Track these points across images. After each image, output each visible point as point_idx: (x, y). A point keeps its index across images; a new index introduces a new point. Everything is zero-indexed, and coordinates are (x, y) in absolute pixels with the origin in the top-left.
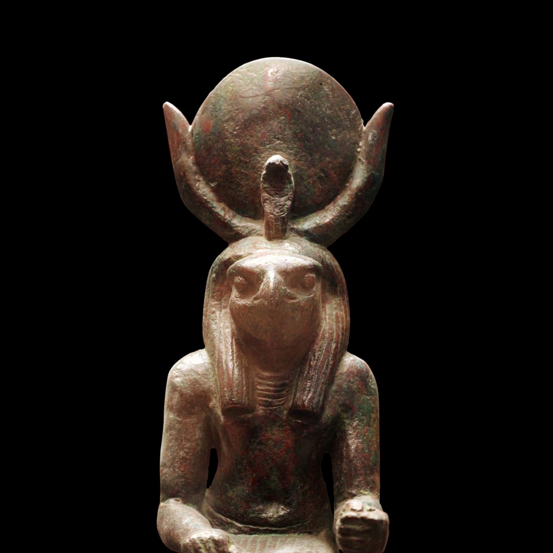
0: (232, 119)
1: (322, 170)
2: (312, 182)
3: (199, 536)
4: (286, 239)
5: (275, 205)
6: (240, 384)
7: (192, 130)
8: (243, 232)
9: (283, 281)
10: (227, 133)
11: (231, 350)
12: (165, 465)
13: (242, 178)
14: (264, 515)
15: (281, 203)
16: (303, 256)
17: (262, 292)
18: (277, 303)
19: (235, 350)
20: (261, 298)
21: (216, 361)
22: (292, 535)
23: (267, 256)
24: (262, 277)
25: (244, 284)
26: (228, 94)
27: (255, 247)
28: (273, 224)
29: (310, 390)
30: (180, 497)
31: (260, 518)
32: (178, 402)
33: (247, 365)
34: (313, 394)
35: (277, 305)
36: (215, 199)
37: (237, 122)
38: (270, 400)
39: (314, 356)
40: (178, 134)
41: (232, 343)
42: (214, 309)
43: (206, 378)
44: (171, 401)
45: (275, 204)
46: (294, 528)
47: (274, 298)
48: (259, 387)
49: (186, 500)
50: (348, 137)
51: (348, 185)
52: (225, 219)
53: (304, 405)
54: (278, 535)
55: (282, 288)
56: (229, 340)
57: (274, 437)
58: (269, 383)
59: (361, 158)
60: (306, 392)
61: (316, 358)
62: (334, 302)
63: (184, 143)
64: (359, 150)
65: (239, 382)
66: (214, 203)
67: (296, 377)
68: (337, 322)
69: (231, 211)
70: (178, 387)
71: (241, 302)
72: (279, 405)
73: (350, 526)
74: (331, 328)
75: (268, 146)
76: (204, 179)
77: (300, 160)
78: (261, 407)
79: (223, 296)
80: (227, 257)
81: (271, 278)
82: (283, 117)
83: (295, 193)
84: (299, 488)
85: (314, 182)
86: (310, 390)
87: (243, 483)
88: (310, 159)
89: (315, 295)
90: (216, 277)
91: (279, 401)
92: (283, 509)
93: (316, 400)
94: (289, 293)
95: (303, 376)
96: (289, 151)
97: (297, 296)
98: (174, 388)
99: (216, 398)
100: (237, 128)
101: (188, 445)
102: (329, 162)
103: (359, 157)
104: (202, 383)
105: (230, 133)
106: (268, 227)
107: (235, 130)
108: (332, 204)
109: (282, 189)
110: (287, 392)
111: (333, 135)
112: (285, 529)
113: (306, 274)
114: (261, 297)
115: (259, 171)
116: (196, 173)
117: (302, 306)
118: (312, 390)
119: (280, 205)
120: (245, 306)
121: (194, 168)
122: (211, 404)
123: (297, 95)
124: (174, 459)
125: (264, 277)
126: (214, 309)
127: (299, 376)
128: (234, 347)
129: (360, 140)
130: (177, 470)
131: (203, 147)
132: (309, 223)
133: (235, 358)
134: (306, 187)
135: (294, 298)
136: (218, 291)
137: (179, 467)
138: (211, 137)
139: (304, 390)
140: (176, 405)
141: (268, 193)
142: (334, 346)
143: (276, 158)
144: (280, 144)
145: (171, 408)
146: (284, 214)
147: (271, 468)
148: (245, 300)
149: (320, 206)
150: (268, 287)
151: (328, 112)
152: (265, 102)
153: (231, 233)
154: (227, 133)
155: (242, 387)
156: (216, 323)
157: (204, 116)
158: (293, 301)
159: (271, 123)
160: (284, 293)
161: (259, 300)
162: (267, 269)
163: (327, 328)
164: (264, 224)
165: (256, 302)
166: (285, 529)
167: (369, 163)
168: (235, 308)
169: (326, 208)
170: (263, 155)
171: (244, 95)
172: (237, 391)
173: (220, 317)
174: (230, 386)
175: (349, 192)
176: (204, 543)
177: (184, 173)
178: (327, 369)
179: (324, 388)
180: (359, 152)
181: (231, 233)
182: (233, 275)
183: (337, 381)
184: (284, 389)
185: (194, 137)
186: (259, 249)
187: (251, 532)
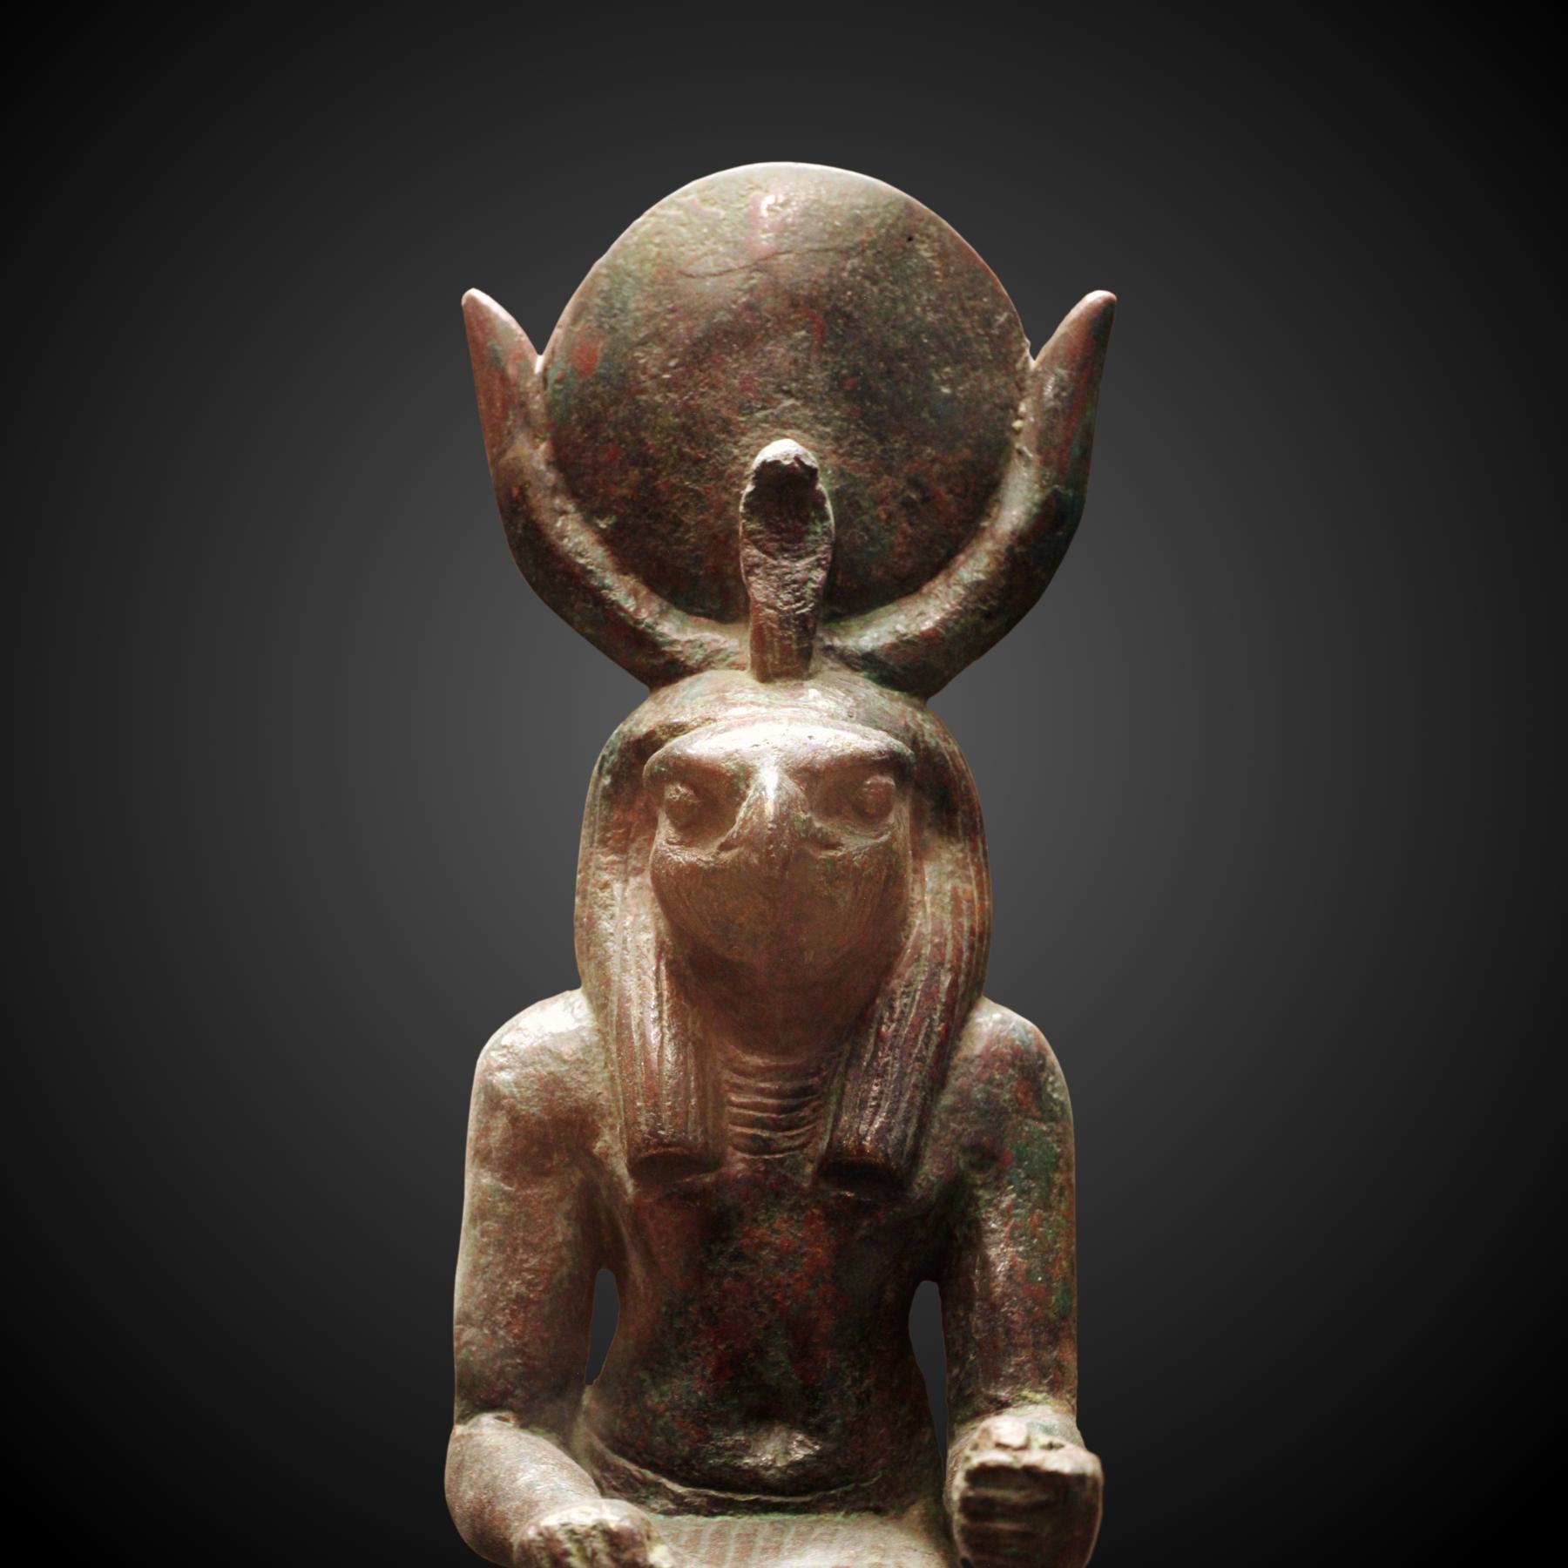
0: (658, 336)
1: (914, 483)
2: (884, 516)
3: (565, 1520)
4: (810, 677)
5: (779, 581)
6: (680, 1090)
7: (545, 369)
8: (688, 658)
9: (802, 796)
10: (643, 378)
11: (654, 993)
12: (467, 1319)
13: (685, 505)
14: (747, 1460)
15: (798, 576)
16: (859, 727)
17: (742, 827)
18: (785, 859)
19: (666, 993)
20: (741, 844)
21: (612, 1022)
22: (828, 1517)
23: (757, 725)
24: (743, 787)
25: (693, 806)
26: (648, 266)
27: (722, 700)
28: (773, 636)
29: (878, 1106)
30: (511, 1408)
31: (738, 1469)
32: (505, 1141)
33: (700, 1035)
34: (887, 1117)
35: (786, 864)
36: (608, 563)
37: (672, 346)
38: (766, 1134)
39: (892, 1009)
40: (504, 379)
41: (657, 972)
42: (606, 877)
43: (585, 1072)
44: (486, 1137)
45: (780, 577)
46: (833, 1498)
47: (778, 844)
48: (733, 1098)
49: (528, 1419)
50: (987, 387)
51: (985, 524)
52: (638, 622)
53: (861, 1149)
54: (788, 1517)
55: (798, 818)
56: (650, 963)
57: (776, 1240)
58: (762, 1085)
59: (1025, 449)
60: (868, 1113)
61: (896, 1016)
62: (946, 856)
63: (523, 405)
64: (1018, 424)
65: (678, 1084)
66: (608, 574)
67: (841, 1069)
68: (957, 912)
69: (654, 597)
70: (505, 1097)
71: (685, 856)
72: (790, 1149)
73: (992, 1493)
74: (938, 931)
75: (760, 415)
76: (579, 509)
77: (850, 454)
78: (739, 1155)
79: (633, 841)
80: (643, 729)
81: (770, 789)
82: (803, 333)
83: (836, 546)
84: (849, 1383)
85: (890, 516)
86: (878, 1106)
87: (689, 1371)
88: (878, 450)
89: (894, 838)
90: (613, 784)
91: (792, 1138)
92: (802, 1444)
93: (895, 1135)
94: (820, 829)
95: (860, 1065)
96: (821, 428)
97: (843, 840)
98: (494, 1101)
99: (612, 1127)
100: (672, 363)
101: (533, 1262)
102: (934, 460)
103: (1017, 445)
104: (573, 1085)
105: (653, 377)
106: (760, 643)
107: (665, 369)
108: (941, 577)
109: (798, 537)
110: (814, 1110)
111: (944, 383)
112: (807, 1499)
113: (866, 778)
114: (741, 841)
115: (733, 484)
116: (555, 491)
117: (855, 869)
118: (886, 1105)
119: (795, 582)
120: (694, 869)
121: (551, 477)
122: (599, 1146)
123: (843, 269)
124: (493, 1301)
125: (748, 787)
126: (606, 877)
127: (848, 1065)
128: (665, 984)
129: (1022, 398)
130: (502, 1333)
131: (575, 417)
132: (875, 634)
133: (665, 1016)
134: (867, 530)
135: (834, 846)
136: (619, 826)
137: (509, 1324)
138: (600, 389)
139: (863, 1105)
140: (499, 1150)
141: (760, 548)
142: (946, 980)
143: (782, 449)
144: (794, 407)
145: (484, 1158)
146: (804, 606)
147: (767, 1327)
148: (694, 851)
149: (906, 585)
150: (761, 814)
151: (931, 317)
152: (751, 290)
153: (654, 662)
154: (643, 378)
155: (687, 1098)
156: (612, 917)
157: (577, 329)
158: (832, 853)
159: (768, 348)
160: (806, 831)
161: (736, 851)
162: (757, 763)
163: (927, 929)
164: (748, 636)
165: (726, 856)
166: (807, 1499)
167: (1046, 462)
168: (668, 874)
169: (925, 590)
170: (745, 440)
171: (691, 269)
172: (671, 1108)
173: (624, 899)
174: (653, 1095)
176: (577, 1541)
177: (522, 490)
178: (927, 1045)
179: (918, 1101)
180: (1017, 432)
181: (654, 662)
182: (660, 780)
183: (956, 1082)
184: (806, 1104)
185: (549, 390)
186: (734, 705)
187: (712, 1508)
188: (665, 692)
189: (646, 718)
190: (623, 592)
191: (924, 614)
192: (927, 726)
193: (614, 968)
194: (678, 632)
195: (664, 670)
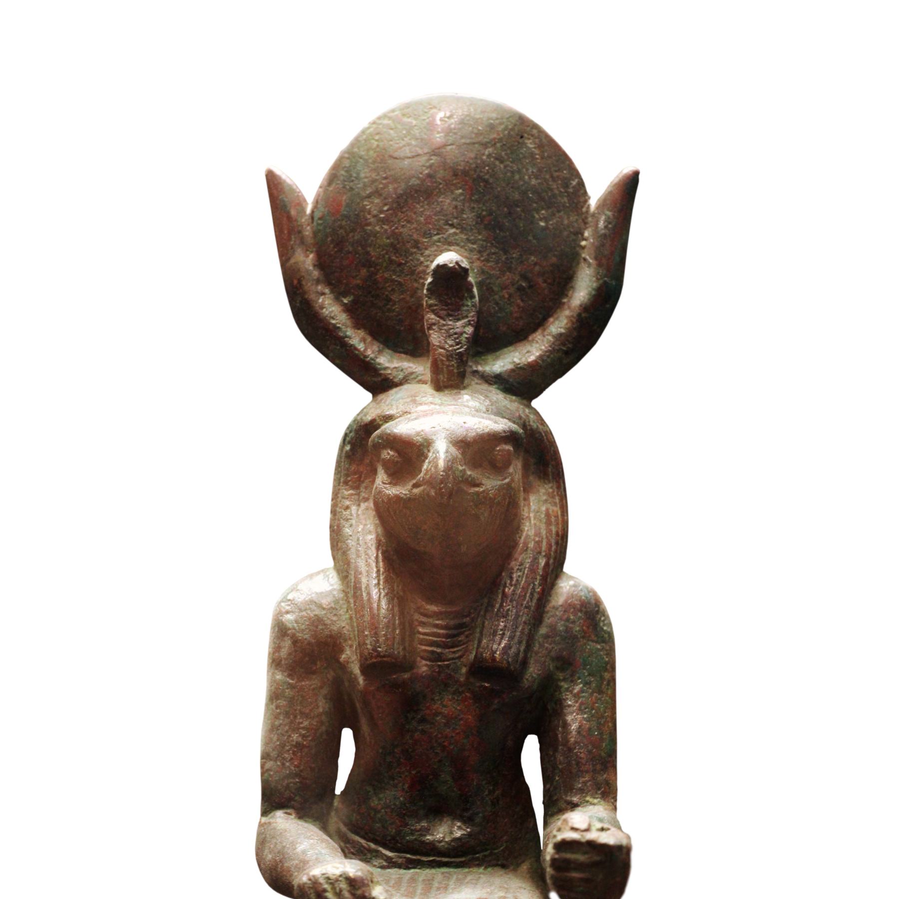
0: (377, 193)
1: (524, 277)
2: (507, 296)
3: (324, 872)
4: (465, 388)
5: (446, 333)
6: (390, 625)
8: (394, 377)
9: (460, 456)
10: (369, 217)
11: (375, 570)
13: (393, 290)
14: (428, 837)
15: (458, 330)
16: (492, 417)
17: (425, 474)
18: (450, 493)
19: (382, 570)
20: (425, 484)
22: (475, 870)
23: (434, 416)
24: (426, 451)
25: (397, 462)
26: (371, 153)
27: (414, 401)
28: (443, 364)
29: (504, 634)
30: (293, 807)
31: (423, 842)
32: (290, 654)
33: (401, 593)
34: (508, 641)
35: (450, 495)
36: (349, 323)
37: (385, 198)
38: (439, 650)
39: (511, 578)
41: (377, 557)
42: (347, 503)
43: (335, 615)
44: (279, 652)
45: (447, 331)
46: (478, 859)
47: (446, 484)
48: (421, 630)
50: (566, 222)
51: (565, 300)
52: (366, 357)
53: (494, 659)
54: (452, 870)
55: (458, 469)
56: (373, 552)
57: (445, 711)
58: (437, 622)
59: (588, 257)
60: (498, 638)
61: (514, 583)
62: (543, 491)
63: (300, 232)
64: (583, 243)
65: (389, 622)
66: (349, 329)
67: (482, 613)
68: (548, 523)
69: (375, 342)
70: (289, 629)
71: (393, 491)
72: (453, 659)
73: (569, 856)
74: (538, 534)
75: (436, 238)
76: (332, 292)
77: (487, 260)
78: (424, 662)
79: (363, 482)
81: (441, 452)
82: (460, 191)
83: (479, 313)
84: (487, 793)
85: (510, 296)
86: (504, 634)
87: (395, 786)
88: (504, 258)
89: (512, 480)
90: (351, 450)
91: (454, 652)
92: (460, 828)
93: (513, 650)
94: (470, 476)
95: (493, 611)
96: (471, 246)
97: (484, 482)
99: (351, 646)
100: (385, 208)
101: (306, 723)
102: (536, 264)
103: (583, 255)
104: (329, 622)
105: (375, 216)
106: (436, 368)
107: (381, 212)
108: (540, 331)
109: (458, 308)
110: (467, 637)
111: (541, 219)
112: (463, 859)
113: (497, 446)
114: (425, 482)
115: (420, 278)
116: (318, 281)
117: (490, 498)
118: (508, 634)
119: (456, 334)
120: (398, 498)
121: (316, 273)
122: (343, 657)
123: (483, 154)
124: (283, 746)
125: (429, 451)
126: (347, 503)
127: (486, 611)
128: (381, 564)
129: (586, 228)
130: (288, 764)
131: (329, 239)
132: (502, 363)
133: (381, 583)
134: (497, 304)
135: (478, 485)
136: (355, 473)
137: (292, 759)
138: (344, 223)
139: (495, 633)
140: (286, 659)
141: (436, 314)
142: (542, 562)
143: (448, 257)
144: (455, 234)
146: (461, 347)
147: (440, 761)
148: (398, 488)
149: (519, 336)
150: (436, 467)
151: (534, 182)
152: (431, 166)
153: (375, 379)
154: (369, 217)
155: (394, 630)
156: (351, 526)
157: (331, 189)
158: (477, 489)
159: (440, 200)
160: (462, 477)
161: (422, 488)
162: (434, 438)
163: (532, 533)
164: (429, 365)
165: (416, 491)
166: (463, 859)
167: (600, 265)
168: (383, 501)
169: (530, 338)
170: (427, 252)
171: (396, 154)
172: (385, 635)
173: (358, 515)
174: (374, 628)
175: (567, 312)
176: (331, 883)
177: (299, 281)
178: (531, 599)
179: (526, 631)
180: (583, 248)
181: (375, 379)
182: (378, 447)
183: (548, 620)
184: (462, 633)
185: (315, 224)
186: (421, 404)
187: (408, 865)
190: (357, 339)
191: (530, 352)
194: (388, 362)
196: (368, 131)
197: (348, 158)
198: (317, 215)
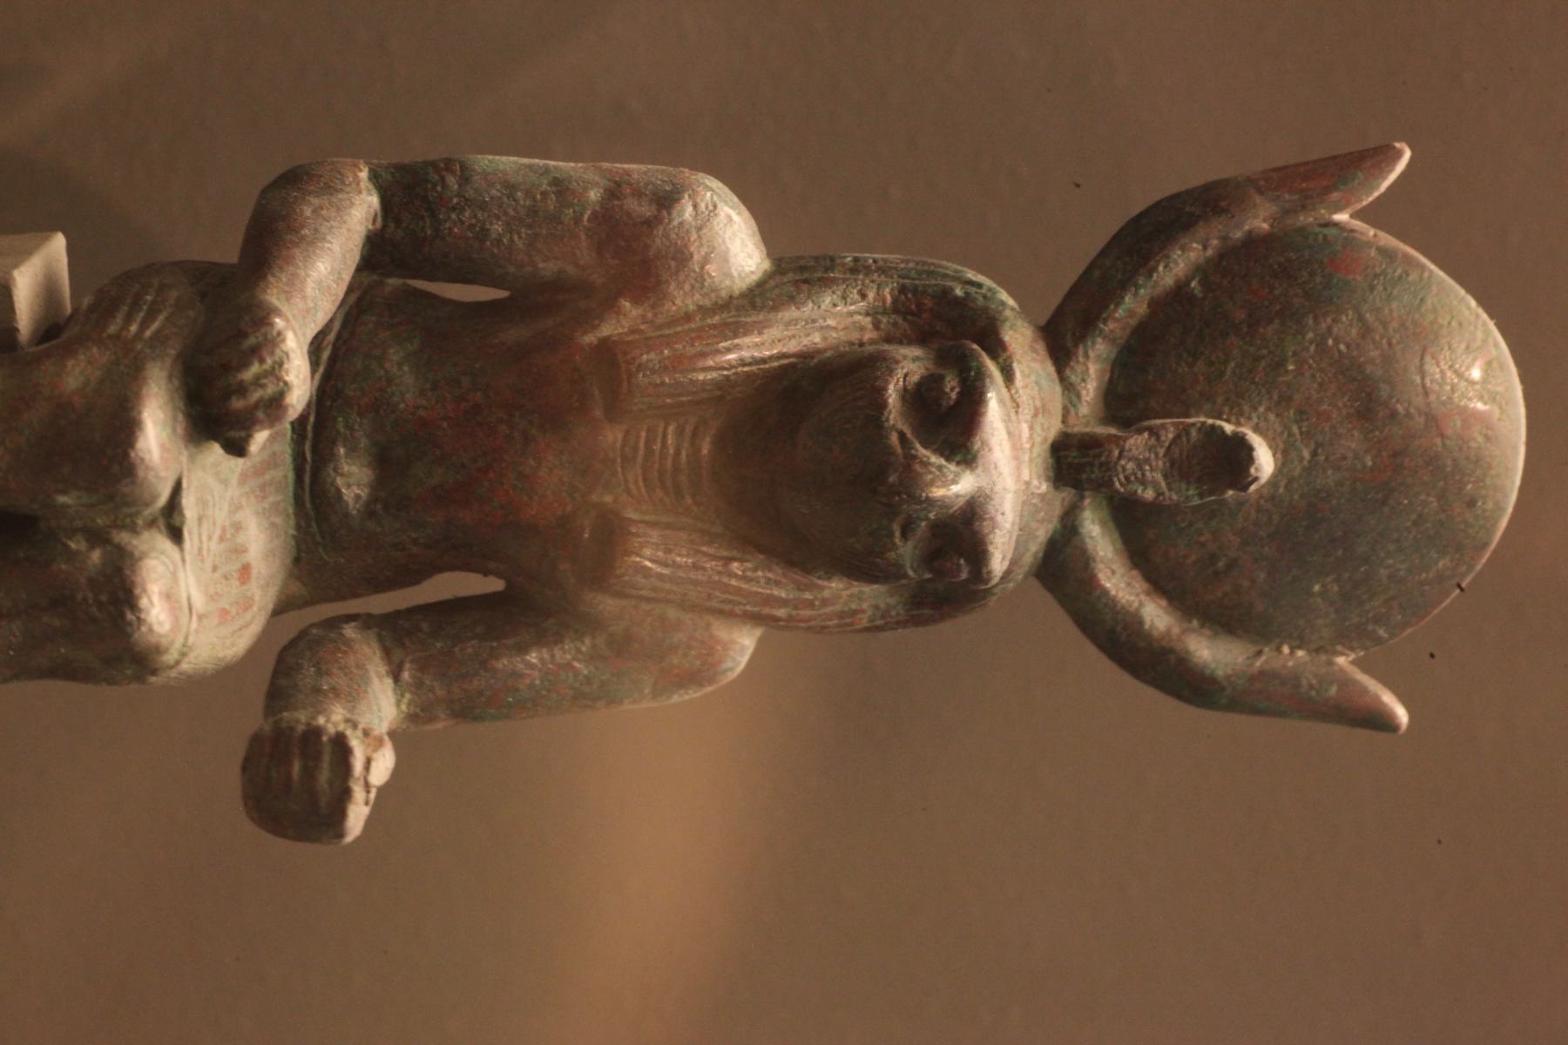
0: (1366, 331)
1: (1232, 564)
2: (1202, 539)
3: (292, 355)
5: (1143, 460)
7: (1336, 224)
8: (1072, 368)
10: (1329, 320)
13: (1211, 363)
14: (342, 451)
22: (292, 522)
23: (1014, 463)
24: (958, 458)
25: (940, 405)
26: (1430, 317)
28: (1095, 457)
30: (385, 226)
31: (334, 443)
32: (629, 214)
36: (1159, 290)
37: (1358, 345)
38: (640, 459)
39: (755, 570)
40: (1327, 190)
42: (871, 295)
43: (693, 287)
44: (633, 195)
45: (1147, 461)
46: (309, 526)
48: (671, 429)
50: (1320, 622)
51: (1195, 623)
53: (628, 553)
54: (291, 488)
56: (792, 347)
57: (543, 472)
58: (684, 454)
59: (1264, 658)
62: (892, 601)
63: (1304, 207)
64: (1286, 649)
66: (1149, 291)
67: (700, 525)
69: (1128, 332)
70: (669, 214)
72: (626, 481)
73: (326, 758)
75: (1295, 429)
76: (1208, 261)
77: (1259, 510)
78: (620, 436)
79: (905, 319)
82: (1370, 463)
84: (414, 535)
85: (1203, 545)
87: (422, 393)
88: (1263, 533)
90: (956, 298)
91: (636, 482)
92: (358, 497)
93: (640, 579)
96: (1283, 484)
97: (910, 544)
98: (666, 200)
100: (1342, 347)
101: (520, 244)
102: (1253, 581)
103: (1266, 649)
104: (682, 277)
105: (1329, 330)
106: (1089, 444)
107: (1337, 341)
108: (1145, 586)
109: (1185, 476)
111: (1323, 586)
112: (308, 505)
114: (911, 458)
115: (1231, 409)
116: (1224, 238)
118: (665, 571)
120: (883, 405)
121: (1238, 235)
122: (626, 304)
123: (1428, 495)
124: (483, 206)
125: (958, 463)
126: (871, 295)
128: (776, 364)
129: (1309, 651)
130: (454, 216)
131: (1293, 256)
134: (1191, 524)
135: (904, 535)
136: (919, 305)
137: (463, 223)
138: (1318, 279)
140: (621, 207)
141: (1174, 441)
143: (1265, 461)
144: (1301, 459)
147: (463, 466)
148: (898, 405)
149: (1139, 556)
150: (932, 483)
151: (1383, 572)
152: (1408, 415)
153: (1069, 337)
154: (1329, 320)
156: (835, 305)
157: (1373, 253)
158: (897, 534)
159: (1356, 433)
161: (899, 450)
162: (979, 471)
165: (894, 438)
166: (308, 505)
167: (1253, 678)
168: (877, 378)
169: (1135, 572)
170: (1272, 417)
171: (1428, 359)
172: (663, 383)
173: (851, 314)
175: (1176, 630)
176: (273, 368)
177: (1225, 211)
178: (723, 601)
179: (671, 597)
180: (1278, 649)
181: (1069, 337)
183: (687, 618)
185: (1317, 229)
186: (1031, 428)
188: (1041, 347)
189: (1019, 337)
190: (1132, 306)
191: (1117, 580)
192: (1011, 585)
193: (791, 313)
194: (1092, 369)
195: (1060, 342)
196: (1463, 308)
197: (1421, 279)
198: (1333, 231)
